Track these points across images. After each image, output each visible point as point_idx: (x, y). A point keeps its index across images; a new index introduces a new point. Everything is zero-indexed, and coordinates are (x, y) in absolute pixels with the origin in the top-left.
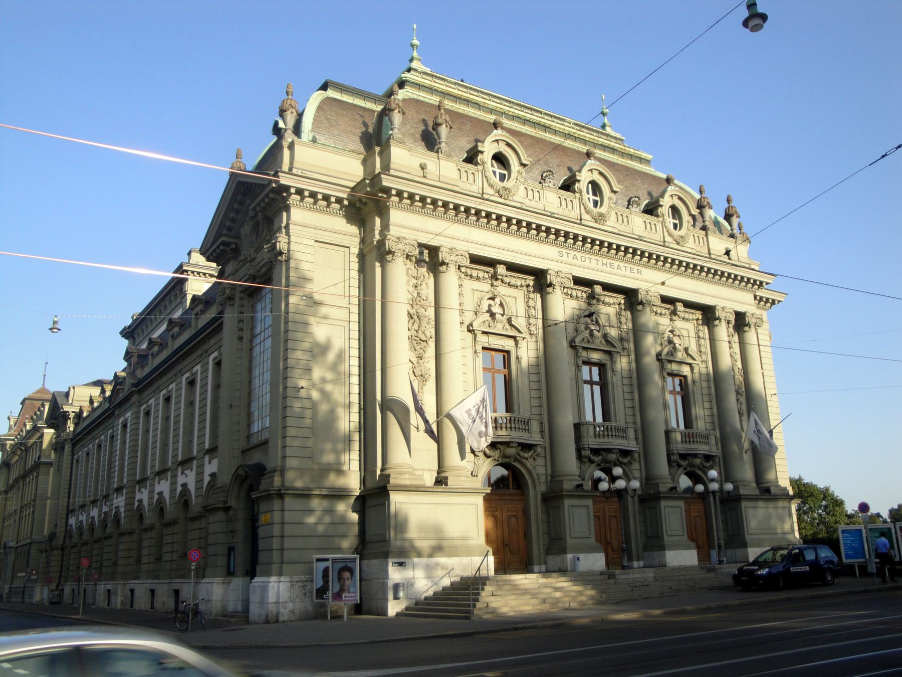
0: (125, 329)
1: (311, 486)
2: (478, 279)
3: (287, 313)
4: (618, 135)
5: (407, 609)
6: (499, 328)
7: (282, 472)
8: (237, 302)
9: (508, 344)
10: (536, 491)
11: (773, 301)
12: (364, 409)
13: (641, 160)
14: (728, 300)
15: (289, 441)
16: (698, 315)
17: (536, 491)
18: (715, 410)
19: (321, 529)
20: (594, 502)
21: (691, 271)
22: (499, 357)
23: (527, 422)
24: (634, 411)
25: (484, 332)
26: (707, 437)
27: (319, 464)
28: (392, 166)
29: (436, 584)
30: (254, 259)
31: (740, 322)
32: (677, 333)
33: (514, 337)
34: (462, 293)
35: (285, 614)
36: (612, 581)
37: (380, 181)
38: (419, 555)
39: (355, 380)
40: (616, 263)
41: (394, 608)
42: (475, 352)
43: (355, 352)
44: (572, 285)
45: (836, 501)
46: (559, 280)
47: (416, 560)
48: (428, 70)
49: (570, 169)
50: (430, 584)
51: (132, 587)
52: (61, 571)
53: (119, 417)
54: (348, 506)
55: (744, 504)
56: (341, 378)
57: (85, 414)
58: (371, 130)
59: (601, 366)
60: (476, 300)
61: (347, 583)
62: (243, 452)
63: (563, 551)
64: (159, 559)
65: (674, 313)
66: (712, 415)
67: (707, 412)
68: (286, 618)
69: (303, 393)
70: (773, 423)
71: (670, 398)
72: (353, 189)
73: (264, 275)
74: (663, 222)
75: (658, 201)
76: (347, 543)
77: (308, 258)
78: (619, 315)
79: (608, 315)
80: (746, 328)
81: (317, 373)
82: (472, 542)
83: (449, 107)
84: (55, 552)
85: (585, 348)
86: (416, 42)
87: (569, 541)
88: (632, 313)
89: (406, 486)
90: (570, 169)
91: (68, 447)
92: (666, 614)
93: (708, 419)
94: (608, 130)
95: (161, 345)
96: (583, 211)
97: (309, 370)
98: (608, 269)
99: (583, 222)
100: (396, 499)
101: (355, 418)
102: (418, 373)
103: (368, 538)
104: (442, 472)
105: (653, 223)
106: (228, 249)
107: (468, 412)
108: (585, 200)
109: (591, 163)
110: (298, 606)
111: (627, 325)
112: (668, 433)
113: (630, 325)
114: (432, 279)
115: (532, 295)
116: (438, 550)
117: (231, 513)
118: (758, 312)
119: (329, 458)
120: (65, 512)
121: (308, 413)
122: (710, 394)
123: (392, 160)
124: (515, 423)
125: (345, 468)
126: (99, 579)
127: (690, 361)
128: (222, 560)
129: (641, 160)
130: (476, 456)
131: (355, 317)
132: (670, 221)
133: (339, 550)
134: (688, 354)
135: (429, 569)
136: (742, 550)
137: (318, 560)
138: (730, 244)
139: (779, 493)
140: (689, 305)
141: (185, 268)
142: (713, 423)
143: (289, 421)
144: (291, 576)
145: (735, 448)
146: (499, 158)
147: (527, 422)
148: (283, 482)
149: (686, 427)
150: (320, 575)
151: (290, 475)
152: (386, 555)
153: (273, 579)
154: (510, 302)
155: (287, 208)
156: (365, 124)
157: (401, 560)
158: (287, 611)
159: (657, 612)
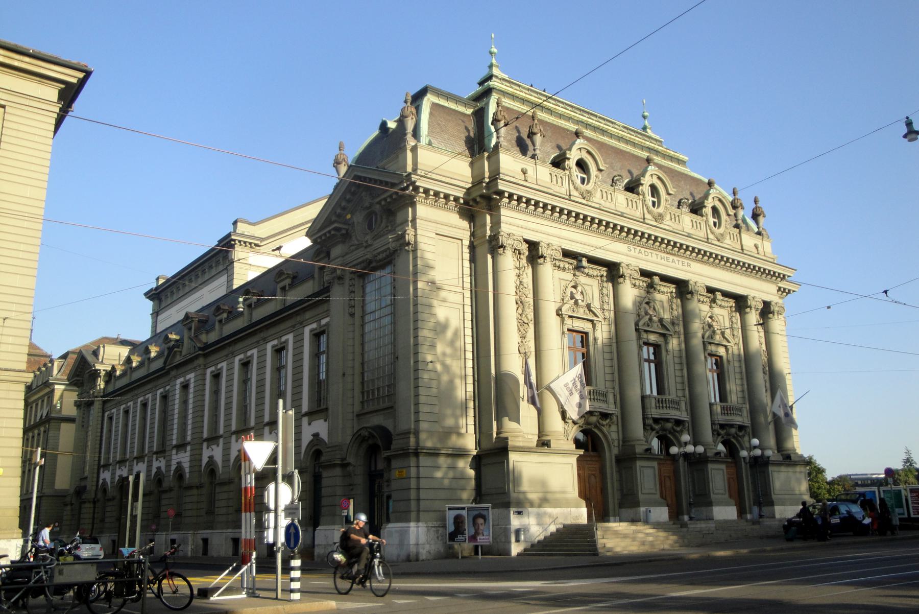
0: (151, 290)
1: (438, 446)
2: (564, 269)
3: (416, 296)
4: (657, 137)
5: (525, 550)
6: (581, 312)
7: (417, 433)
9: (587, 327)
10: (611, 453)
11: (789, 291)
12: (478, 381)
13: (679, 161)
14: (758, 290)
15: (422, 408)
16: (732, 303)
17: (611, 453)
18: (746, 386)
19: (446, 482)
20: (659, 464)
21: (632, 236)
22: (578, 337)
23: (605, 395)
25: (570, 316)
26: (740, 410)
27: (443, 427)
28: (501, 171)
29: (545, 530)
30: (371, 245)
31: (766, 310)
32: (715, 318)
33: (592, 321)
34: (554, 280)
35: (423, 554)
36: (685, 529)
37: (497, 185)
38: (532, 505)
39: (469, 355)
40: (671, 257)
41: (516, 549)
42: (563, 333)
43: (469, 332)
44: (561, 257)
45: (819, 469)
46: (629, 272)
47: (530, 509)
48: (506, 77)
49: (559, 147)
50: (541, 530)
51: (205, 536)
52: (93, 523)
53: (176, 378)
54: (466, 463)
55: (771, 468)
56: (458, 353)
57: (118, 373)
58: (472, 134)
59: (657, 347)
60: (562, 288)
61: (481, 527)
62: (358, 416)
63: (637, 504)
64: (102, 521)
65: (714, 301)
66: (743, 391)
67: (739, 388)
68: (424, 557)
69: (430, 366)
70: (791, 400)
71: (709, 374)
72: (468, 189)
73: (380, 260)
74: (644, 201)
75: (639, 180)
76: (467, 494)
77: (431, 249)
78: (670, 301)
79: (662, 302)
80: (771, 316)
81: (440, 348)
82: (569, 496)
83: (507, 105)
84: (87, 505)
85: (646, 331)
86: (494, 50)
87: (641, 497)
88: (682, 301)
89: (522, 447)
90: (559, 147)
91: (97, 406)
92: (751, 552)
93: (740, 394)
94: (650, 132)
95: (230, 312)
96: (646, 211)
97: (433, 346)
98: (665, 262)
99: (572, 198)
100: (513, 457)
101: (470, 388)
102: (522, 351)
103: (484, 489)
104: (543, 436)
105: (559, 176)
106: (338, 234)
107: (566, 385)
108: (575, 178)
109: (580, 142)
110: (433, 547)
111: (678, 311)
112: (711, 405)
113: (680, 310)
114: (530, 270)
115: (605, 285)
116: (544, 501)
117: (350, 468)
118: (781, 301)
119: (450, 422)
120: (96, 467)
121: (434, 384)
122: (741, 373)
123: (501, 165)
124: (595, 396)
125: (463, 431)
126: (157, 530)
127: (725, 343)
129: (679, 161)
130: (566, 422)
131: (468, 301)
132: (649, 199)
133: (460, 500)
134: (724, 337)
135: (539, 516)
136: (769, 508)
137: (450, 509)
138: (757, 240)
139: (797, 459)
140: (593, 261)
141: (233, 237)
142: (744, 397)
143: (422, 391)
144: (426, 522)
145: (762, 419)
146: (581, 164)
147: (605, 395)
148: (417, 442)
149: (658, 393)
150: (452, 521)
151: (423, 436)
152: (507, 505)
153: (412, 524)
154: (588, 289)
155: (413, 205)
156: (467, 129)
157: (520, 510)
158: (424, 552)
159: (744, 551)
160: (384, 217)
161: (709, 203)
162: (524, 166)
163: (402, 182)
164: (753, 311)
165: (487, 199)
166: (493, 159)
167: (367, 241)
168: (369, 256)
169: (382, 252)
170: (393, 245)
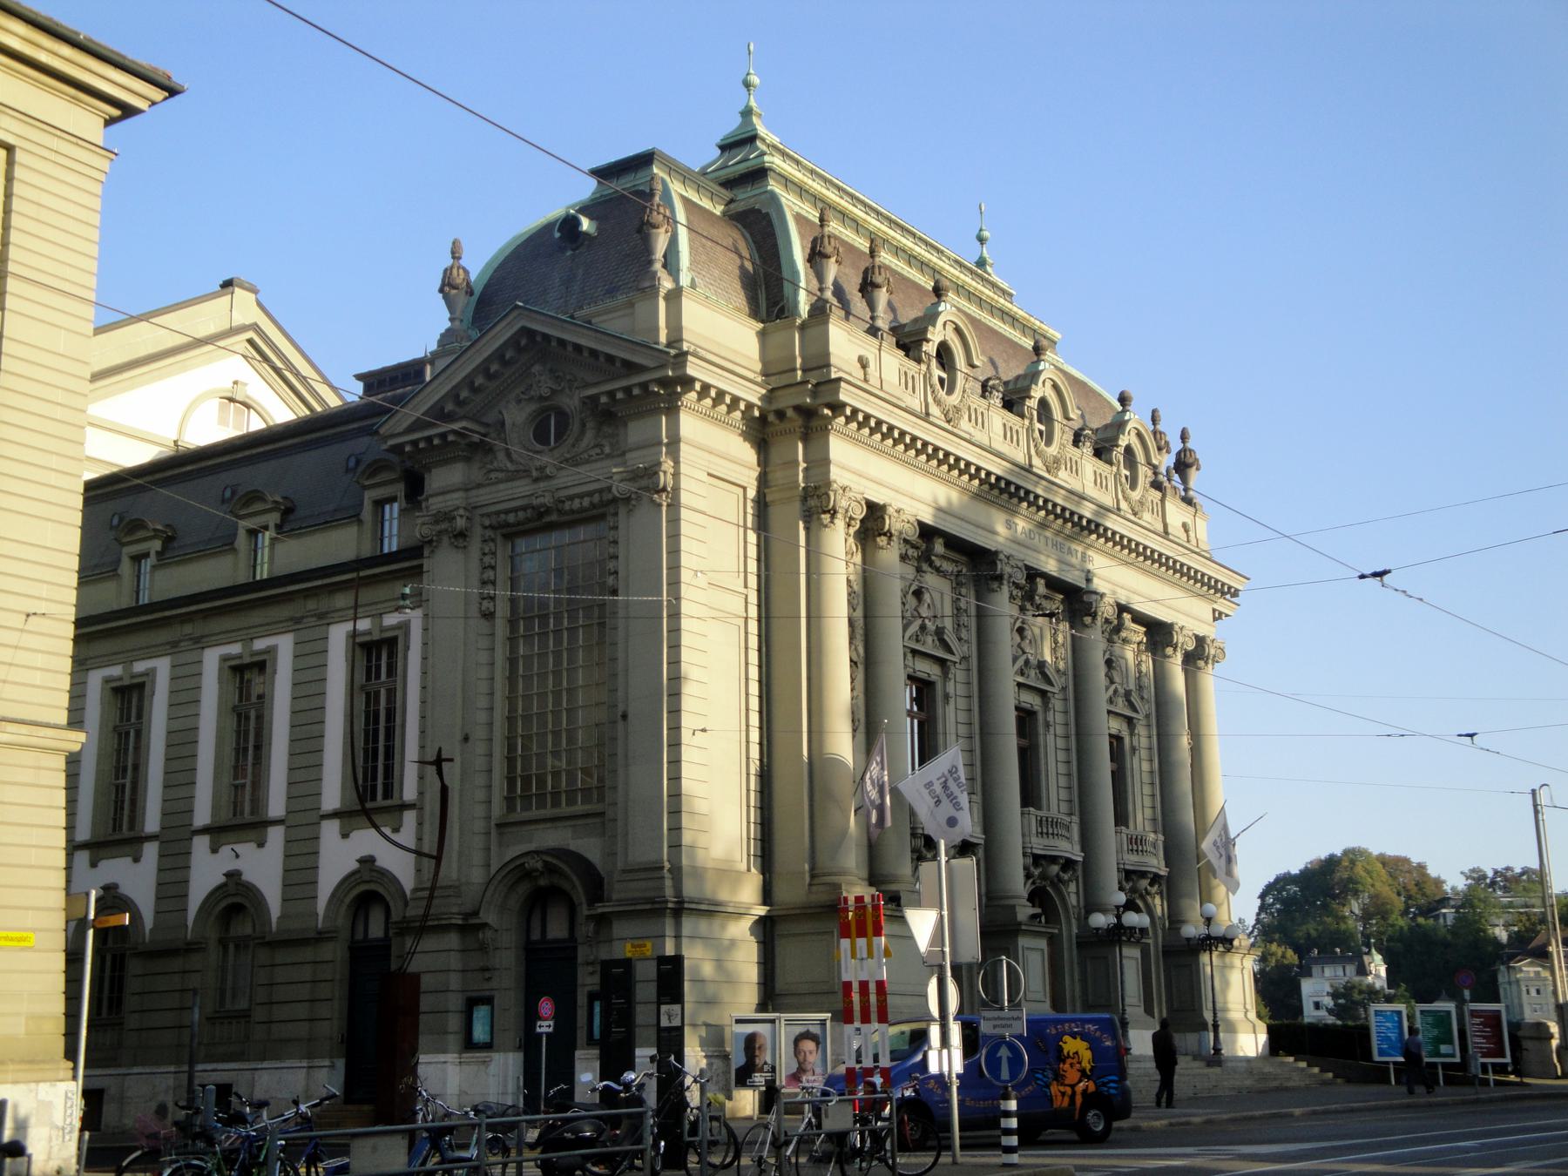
8: (475, 546)
24: (493, 672)
28: (833, 360)
30: (548, 477)
37: (837, 392)
103: (780, 985)
128: (454, 1022)
131: (753, 612)
155: (673, 411)
160: (590, 425)
161: (936, 335)
162: (863, 352)
163: (662, 366)
164: (840, 523)
165: (808, 413)
166: (813, 332)
167: (541, 469)
168: (547, 500)
169: (581, 496)
170: (624, 486)
